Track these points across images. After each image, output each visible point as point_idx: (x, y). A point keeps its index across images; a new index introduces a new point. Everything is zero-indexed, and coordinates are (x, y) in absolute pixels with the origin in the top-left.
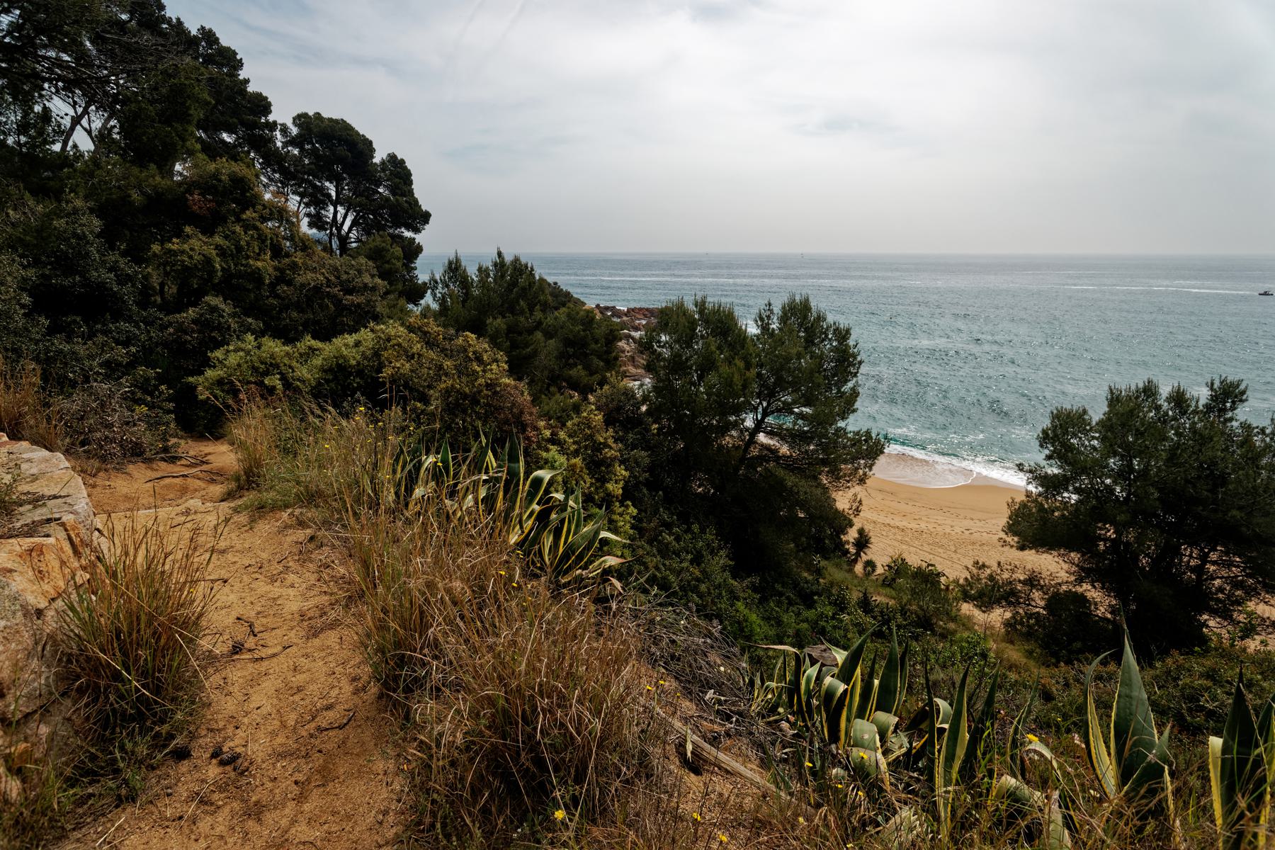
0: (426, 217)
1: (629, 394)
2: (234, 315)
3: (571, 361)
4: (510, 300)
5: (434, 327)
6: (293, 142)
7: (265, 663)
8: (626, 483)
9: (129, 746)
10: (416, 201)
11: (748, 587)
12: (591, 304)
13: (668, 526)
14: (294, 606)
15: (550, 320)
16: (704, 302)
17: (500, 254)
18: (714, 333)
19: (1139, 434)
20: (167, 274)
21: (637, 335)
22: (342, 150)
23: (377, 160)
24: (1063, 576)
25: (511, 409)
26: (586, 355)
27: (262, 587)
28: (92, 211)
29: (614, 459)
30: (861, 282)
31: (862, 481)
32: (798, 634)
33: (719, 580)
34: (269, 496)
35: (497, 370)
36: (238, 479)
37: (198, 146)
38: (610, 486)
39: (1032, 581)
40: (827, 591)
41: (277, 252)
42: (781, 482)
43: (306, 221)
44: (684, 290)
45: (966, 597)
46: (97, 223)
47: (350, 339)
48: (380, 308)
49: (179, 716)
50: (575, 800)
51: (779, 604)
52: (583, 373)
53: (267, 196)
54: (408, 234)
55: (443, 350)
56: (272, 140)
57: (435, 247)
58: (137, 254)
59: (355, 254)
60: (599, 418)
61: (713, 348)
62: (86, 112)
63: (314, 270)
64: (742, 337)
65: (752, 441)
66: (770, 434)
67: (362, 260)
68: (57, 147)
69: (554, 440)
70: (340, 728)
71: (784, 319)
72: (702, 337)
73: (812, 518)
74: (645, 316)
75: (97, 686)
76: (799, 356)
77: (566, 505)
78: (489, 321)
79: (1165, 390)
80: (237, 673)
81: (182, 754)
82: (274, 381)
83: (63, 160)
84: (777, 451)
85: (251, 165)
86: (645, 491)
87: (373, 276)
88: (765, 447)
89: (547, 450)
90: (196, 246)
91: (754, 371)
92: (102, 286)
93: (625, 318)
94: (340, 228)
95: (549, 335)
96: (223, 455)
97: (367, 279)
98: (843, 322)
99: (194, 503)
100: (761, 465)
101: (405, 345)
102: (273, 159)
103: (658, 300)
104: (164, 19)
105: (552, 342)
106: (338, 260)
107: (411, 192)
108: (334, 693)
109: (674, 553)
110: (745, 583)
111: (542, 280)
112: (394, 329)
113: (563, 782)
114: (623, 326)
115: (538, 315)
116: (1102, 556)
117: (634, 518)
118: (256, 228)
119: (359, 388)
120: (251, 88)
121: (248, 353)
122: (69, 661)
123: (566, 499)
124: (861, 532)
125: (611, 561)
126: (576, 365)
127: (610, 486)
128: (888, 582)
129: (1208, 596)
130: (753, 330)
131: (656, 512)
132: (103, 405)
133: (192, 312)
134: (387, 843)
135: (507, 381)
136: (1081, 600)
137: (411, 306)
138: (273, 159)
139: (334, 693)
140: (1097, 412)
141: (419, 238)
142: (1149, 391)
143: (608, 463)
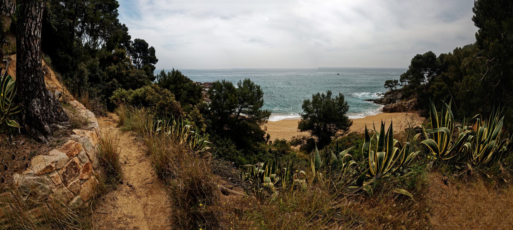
0: (157, 60)
1: (205, 105)
4: (176, 81)
5: (158, 87)
6: (133, 45)
7: (132, 167)
12: (195, 81)
13: (218, 139)
14: (134, 155)
15: (185, 86)
19: (318, 104)
21: (207, 89)
22: (142, 46)
23: (149, 48)
24: (309, 135)
29: (203, 122)
30: (261, 75)
31: (267, 122)
32: (255, 161)
33: (233, 151)
35: (172, 98)
36: (119, 123)
38: (202, 129)
39: (304, 138)
40: (261, 150)
41: (127, 69)
42: (247, 125)
44: (218, 78)
45: (292, 145)
47: (139, 90)
50: (204, 202)
51: (249, 155)
54: (153, 64)
55: (160, 93)
57: (159, 68)
58: (104, 70)
59: (142, 69)
64: (234, 89)
65: (238, 115)
66: (243, 113)
67: (143, 71)
69: (187, 117)
71: (244, 84)
73: (256, 133)
79: (321, 94)
81: (122, 183)
82: (124, 99)
83: (97, 50)
90: (113, 67)
91: (237, 98)
92: (97, 76)
95: (184, 90)
96: (115, 117)
97: (144, 75)
98: (258, 84)
99: (112, 127)
102: (129, 48)
103: (212, 81)
106: (138, 71)
112: (149, 88)
113: (200, 198)
114: (203, 87)
115: (182, 84)
116: (315, 129)
120: (128, 34)
124: (268, 134)
125: (208, 148)
127: (202, 129)
128: (275, 145)
129: (331, 133)
130: (237, 87)
131: (214, 135)
133: (110, 82)
136: (312, 139)
138: (129, 48)
140: (311, 100)
141: (155, 65)
142: (318, 94)
143: (201, 123)
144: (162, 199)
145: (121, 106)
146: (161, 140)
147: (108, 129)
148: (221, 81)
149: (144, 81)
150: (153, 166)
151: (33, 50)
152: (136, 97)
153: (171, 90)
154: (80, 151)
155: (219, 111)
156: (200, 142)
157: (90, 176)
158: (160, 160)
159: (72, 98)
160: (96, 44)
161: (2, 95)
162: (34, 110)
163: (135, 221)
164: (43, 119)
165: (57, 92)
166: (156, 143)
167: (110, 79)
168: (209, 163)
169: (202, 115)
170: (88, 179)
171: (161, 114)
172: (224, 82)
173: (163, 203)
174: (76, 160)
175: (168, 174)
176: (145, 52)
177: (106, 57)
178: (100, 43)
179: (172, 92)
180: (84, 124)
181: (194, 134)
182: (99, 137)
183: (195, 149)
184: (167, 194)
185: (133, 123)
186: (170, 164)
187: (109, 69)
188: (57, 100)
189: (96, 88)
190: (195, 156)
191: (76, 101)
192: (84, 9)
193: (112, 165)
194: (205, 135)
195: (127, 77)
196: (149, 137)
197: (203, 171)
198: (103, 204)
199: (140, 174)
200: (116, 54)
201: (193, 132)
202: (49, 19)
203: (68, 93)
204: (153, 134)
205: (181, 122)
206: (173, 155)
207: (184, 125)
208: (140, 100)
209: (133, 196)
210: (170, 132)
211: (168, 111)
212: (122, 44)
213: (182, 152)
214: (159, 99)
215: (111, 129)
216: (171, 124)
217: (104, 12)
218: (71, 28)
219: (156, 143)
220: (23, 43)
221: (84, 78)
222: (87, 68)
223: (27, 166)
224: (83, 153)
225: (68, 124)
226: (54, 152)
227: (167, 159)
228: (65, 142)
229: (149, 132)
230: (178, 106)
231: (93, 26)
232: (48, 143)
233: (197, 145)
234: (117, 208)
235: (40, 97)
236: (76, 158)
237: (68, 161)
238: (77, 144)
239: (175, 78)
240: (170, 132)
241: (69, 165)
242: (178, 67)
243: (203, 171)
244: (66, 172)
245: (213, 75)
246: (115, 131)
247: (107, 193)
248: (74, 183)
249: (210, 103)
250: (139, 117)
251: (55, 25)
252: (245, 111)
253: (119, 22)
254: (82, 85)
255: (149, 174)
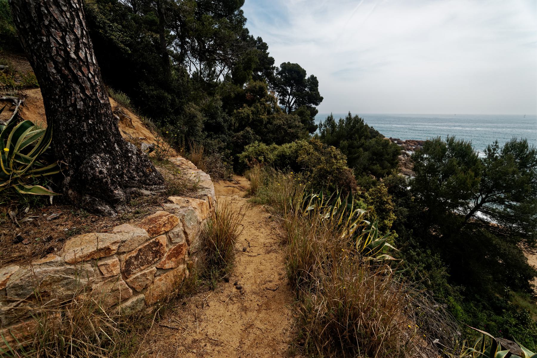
0: (321, 99)
1: (402, 181)
2: (253, 134)
3: (374, 162)
4: (353, 134)
5: (319, 143)
7: (252, 258)
8: (395, 222)
9: (214, 272)
10: (319, 93)
11: (457, 290)
13: (414, 247)
14: (262, 240)
15: (367, 144)
16: (452, 139)
17: (349, 114)
18: (457, 156)
20: (237, 120)
21: (410, 153)
22: (295, 75)
23: (306, 78)
25: (345, 180)
26: (382, 160)
27: (253, 231)
28: (221, 99)
29: (390, 210)
34: (258, 199)
35: (342, 163)
36: (249, 191)
37: (252, 77)
38: (386, 222)
41: (269, 113)
43: (279, 101)
44: (442, 133)
46: (222, 103)
47: (288, 145)
48: (300, 135)
49: (228, 267)
52: (379, 168)
53: (269, 93)
54: (313, 106)
55: (322, 152)
56: (273, 73)
57: (323, 111)
58: (230, 114)
59: (294, 113)
60: (385, 190)
61: (455, 163)
62: (224, 69)
63: (280, 119)
64: (475, 160)
66: (486, 213)
67: (296, 116)
68: (215, 80)
69: (362, 196)
70: (274, 291)
71: (506, 150)
72: (449, 157)
74: (415, 144)
75: (210, 250)
76: (514, 173)
77: (371, 227)
78: (341, 142)
80: (244, 258)
81: (227, 280)
82: (261, 158)
83: (216, 84)
84: (489, 223)
85: (265, 83)
86: (403, 227)
87: (299, 122)
88: (479, 219)
89: (359, 200)
90: (246, 110)
92: (219, 123)
93: (404, 145)
94: (289, 104)
95: (366, 150)
96: (244, 182)
97: (297, 123)
99: (236, 196)
100: (476, 228)
101: (308, 149)
102: (272, 80)
103: (423, 138)
104: (248, 36)
105: (367, 153)
106: (288, 116)
107: (317, 89)
108: (272, 277)
109: (415, 261)
110: (456, 288)
111: (367, 125)
112: (304, 143)
114: (403, 148)
115: (363, 141)
117: (396, 238)
118: (264, 104)
119: (289, 164)
121: (255, 147)
122: (204, 240)
123: (371, 224)
125: (388, 257)
126: (376, 164)
127: (386, 222)
131: (408, 239)
132: (216, 161)
133: (241, 133)
134: (286, 343)
135: (346, 168)
137: (310, 134)
138: (272, 80)
139: (272, 277)
141: (317, 108)
143: (387, 211)
144: (281, 323)
145: (256, 168)
146: (310, 225)
147: (229, 198)
148: (444, 140)
149: (297, 133)
150: (285, 263)
151: (84, 82)
152: (282, 157)
153: (342, 150)
154: (173, 227)
155: (428, 197)
156: (377, 243)
157: (178, 264)
158: (301, 256)
159: (175, 153)
160: (212, 75)
161: (7, 150)
162: (93, 168)
163: (219, 352)
164: (113, 183)
165: (145, 145)
166: (301, 228)
167: (241, 127)
168: (383, 285)
169: (390, 197)
170: (172, 269)
171: (319, 184)
172: (451, 141)
173: (280, 331)
174: (163, 239)
175: (306, 283)
176: (300, 84)
177: (233, 95)
178: (221, 71)
179: (343, 152)
180: (193, 190)
181: (369, 227)
182: (212, 209)
183: (365, 252)
184: (292, 316)
185: (271, 194)
186: (314, 266)
187: (239, 113)
188: (146, 156)
189: (216, 141)
190: (361, 264)
191: (180, 158)
192: (176, 13)
193: (221, 251)
194: (388, 232)
195: (269, 126)
196: (293, 218)
197: (369, 296)
198: (180, 312)
199: (261, 271)
200: (250, 90)
201: (368, 223)
202: (106, 32)
203: (166, 146)
204: (300, 213)
205: (350, 202)
206: (323, 252)
207: (355, 208)
208: (288, 161)
209: (236, 306)
210: (327, 216)
211: (332, 181)
212: (260, 73)
213: (340, 251)
214: (319, 161)
215: (234, 199)
216: (333, 202)
217: (218, 17)
218: (160, 47)
219: (301, 228)
220: (54, 71)
221: (196, 126)
222: (201, 111)
223: (50, 251)
224: (178, 229)
225: (162, 189)
226: (126, 227)
227: (311, 256)
228: (149, 214)
229: (294, 210)
230: (350, 176)
231: (202, 43)
232: (114, 215)
233: (371, 247)
234: (201, 321)
235: (109, 150)
236: (164, 236)
237: (147, 241)
238: (172, 217)
239: (351, 129)
240: (327, 216)
241: (145, 247)
242: (358, 110)
243: (369, 296)
244: (136, 258)
245: (428, 126)
246: (240, 202)
247: (196, 294)
248: (144, 275)
249: (412, 178)
250: (282, 185)
251: (122, 42)
252: (493, 210)
253: (250, 34)
254: (192, 135)
255: (276, 274)
